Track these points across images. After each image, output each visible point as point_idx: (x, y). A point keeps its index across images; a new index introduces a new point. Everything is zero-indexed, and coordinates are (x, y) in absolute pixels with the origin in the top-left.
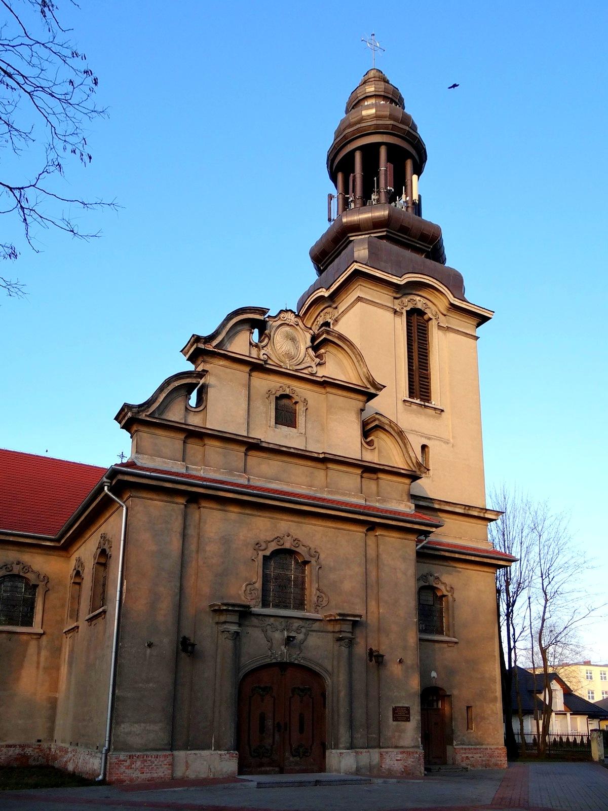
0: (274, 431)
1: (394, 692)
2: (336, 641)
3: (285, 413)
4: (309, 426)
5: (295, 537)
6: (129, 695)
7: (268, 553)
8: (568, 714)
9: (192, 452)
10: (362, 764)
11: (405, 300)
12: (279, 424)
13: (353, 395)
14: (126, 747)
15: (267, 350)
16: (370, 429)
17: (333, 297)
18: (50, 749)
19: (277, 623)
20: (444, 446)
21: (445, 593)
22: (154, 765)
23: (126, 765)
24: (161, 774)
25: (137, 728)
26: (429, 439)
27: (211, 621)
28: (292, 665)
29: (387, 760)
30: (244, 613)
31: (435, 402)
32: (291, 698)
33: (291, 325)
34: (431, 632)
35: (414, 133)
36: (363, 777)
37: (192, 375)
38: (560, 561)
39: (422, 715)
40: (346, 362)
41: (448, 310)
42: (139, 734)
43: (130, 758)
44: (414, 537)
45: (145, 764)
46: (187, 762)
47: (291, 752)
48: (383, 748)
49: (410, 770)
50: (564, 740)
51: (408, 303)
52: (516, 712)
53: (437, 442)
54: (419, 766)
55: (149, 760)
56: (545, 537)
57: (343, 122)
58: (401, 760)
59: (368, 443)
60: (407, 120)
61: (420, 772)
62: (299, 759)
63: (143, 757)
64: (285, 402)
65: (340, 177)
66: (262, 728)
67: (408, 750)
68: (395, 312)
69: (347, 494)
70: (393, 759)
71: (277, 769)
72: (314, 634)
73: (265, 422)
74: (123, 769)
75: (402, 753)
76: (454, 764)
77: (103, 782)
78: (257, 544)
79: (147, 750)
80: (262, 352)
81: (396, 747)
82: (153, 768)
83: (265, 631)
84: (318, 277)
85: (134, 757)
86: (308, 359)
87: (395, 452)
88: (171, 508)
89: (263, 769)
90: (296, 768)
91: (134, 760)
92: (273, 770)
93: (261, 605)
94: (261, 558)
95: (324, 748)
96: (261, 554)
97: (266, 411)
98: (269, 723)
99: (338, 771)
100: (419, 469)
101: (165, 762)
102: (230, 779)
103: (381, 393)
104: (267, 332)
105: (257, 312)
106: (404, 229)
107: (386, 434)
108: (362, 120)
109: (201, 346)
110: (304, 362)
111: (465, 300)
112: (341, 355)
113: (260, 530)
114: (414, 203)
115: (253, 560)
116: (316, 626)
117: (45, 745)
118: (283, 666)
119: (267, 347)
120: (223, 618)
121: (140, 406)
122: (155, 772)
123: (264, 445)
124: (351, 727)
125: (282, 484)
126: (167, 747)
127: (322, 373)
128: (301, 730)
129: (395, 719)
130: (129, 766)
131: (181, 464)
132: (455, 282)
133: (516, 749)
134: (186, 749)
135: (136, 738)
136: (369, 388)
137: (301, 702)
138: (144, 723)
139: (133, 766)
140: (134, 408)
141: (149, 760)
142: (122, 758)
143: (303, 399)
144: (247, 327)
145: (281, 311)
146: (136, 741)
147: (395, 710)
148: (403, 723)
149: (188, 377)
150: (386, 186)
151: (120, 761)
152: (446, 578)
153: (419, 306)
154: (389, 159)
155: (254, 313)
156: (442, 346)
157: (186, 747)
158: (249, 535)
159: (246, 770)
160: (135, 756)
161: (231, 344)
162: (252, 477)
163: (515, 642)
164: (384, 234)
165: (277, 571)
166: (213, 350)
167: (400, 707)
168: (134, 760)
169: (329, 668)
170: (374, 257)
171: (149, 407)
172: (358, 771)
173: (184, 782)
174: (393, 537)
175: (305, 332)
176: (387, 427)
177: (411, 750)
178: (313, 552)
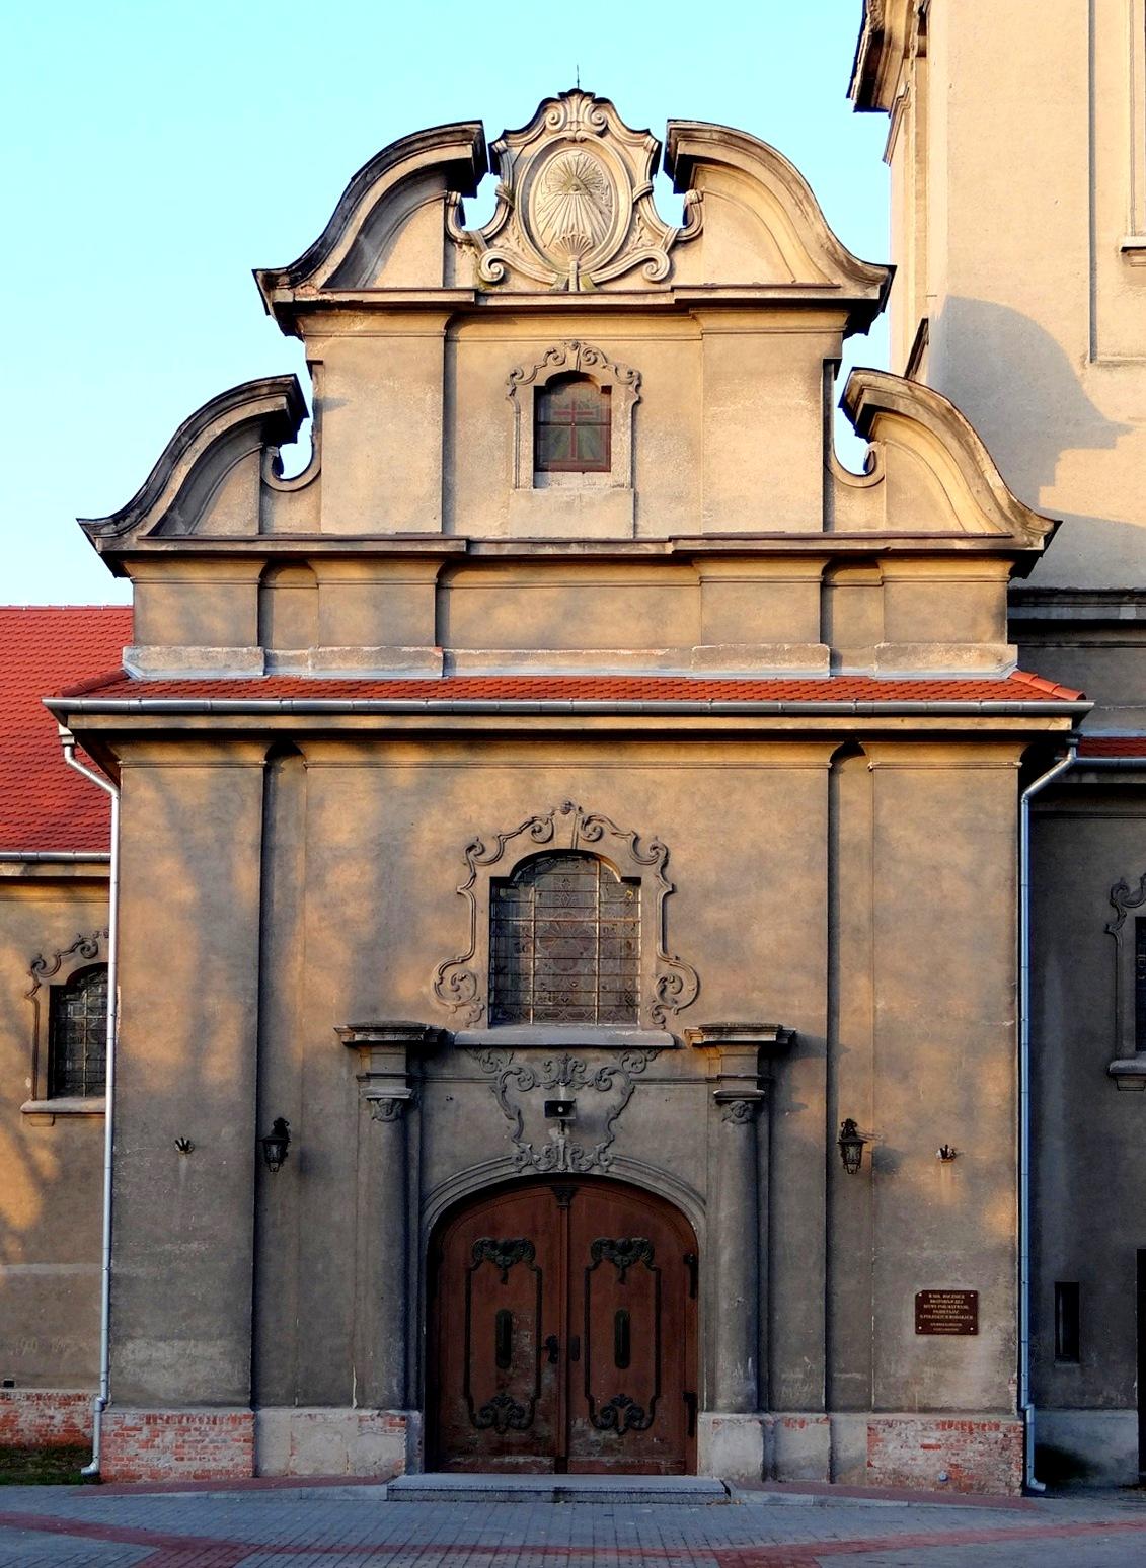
0: (530, 497)
1: (922, 1249)
2: (715, 1107)
4: (646, 455)
5: (588, 812)
6: (141, 1272)
7: (503, 869)
9: (290, 609)
10: (803, 1454)
12: (553, 470)
19: (538, 1067)
22: (207, 1440)
23: (140, 1439)
24: (226, 1464)
25: (165, 1352)
27: (345, 1074)
28: (584, 1178)
29: (890, 1448)
30: (427, 1050)
32: (588, 1270)
33: (583, 140)
37: (256, 392)
42: (171, 1367)
43: (148, 1423)
45: (186, 1437)
47: (593, 1419)
48: (877, 1410)
49: (971, 1477)
54: (1004, 1466)
55: (195, 1429)
58: (939, 1447)
61: (1007, 1484)
62: (615, 1436)
63: (180, 1422)
66: (505, 1354)
67: (966, 1418)
69: (765, 651)
70: (911, 1443)
71: (547, 1461)
72: (652, 1087)
73: (502, 475)
74: (132, 1448)
75: (943, 1426)
78: (471, 848)
79: (192, 1404)
82: (206, 1447)
85: (159, 1421)
88: (228, 779)
89: (507, 1459)
90: (605, 1459)
91: (158, 1427)
92: (534, 1463)
93: (485, 1018)
94: (483, 889)
96: (485, 874)
98: (525, 1341)
100: (1025, 525)
101: (236, 1435)
105: (448, 138)
107: (909, 428)
110: (627, 250)
112: (749, 196)
113: (482, 807)
115: (459, 893)
116: (659, 1066)
118: (565, 1185)
119: (504, 234)
120: (368, 1064)
121: (118, 517)
122: (211, 1457)
123: (484, 550)
125: (555, 656)
126: (238, 1399)
128: (623, 1358)
129: (925, 1327)
130: (148, 1442)
131: (250, 653)
134: (291, 1404)
135: (164, 1374)
136: (838, 287)
137: (622, 1281)
138: (181, 1338)
139: (158, 1441)
140: (104, 526)
141: (195, 1429)
142: (129, 1422)
143: (623, 374)
144: (434, 189)
145: (545, 104)
146: (161, 1382)
147: (922, 1300)
148: (953, 1339)
149: (247, 402)
151: (127, 1429)
155: (440, 145)
158: (449, 825)
159: (459, 1459)
160: (161, 1419)
161: (386, 260)
162: (462, 651)
166: (320, 297)
167: (942, 1293)
168: (158, 1427)
169: (700, 1185)
171: (145, 513)
174: (931, 767)
175: (629, 148)
177: (976, 1419)
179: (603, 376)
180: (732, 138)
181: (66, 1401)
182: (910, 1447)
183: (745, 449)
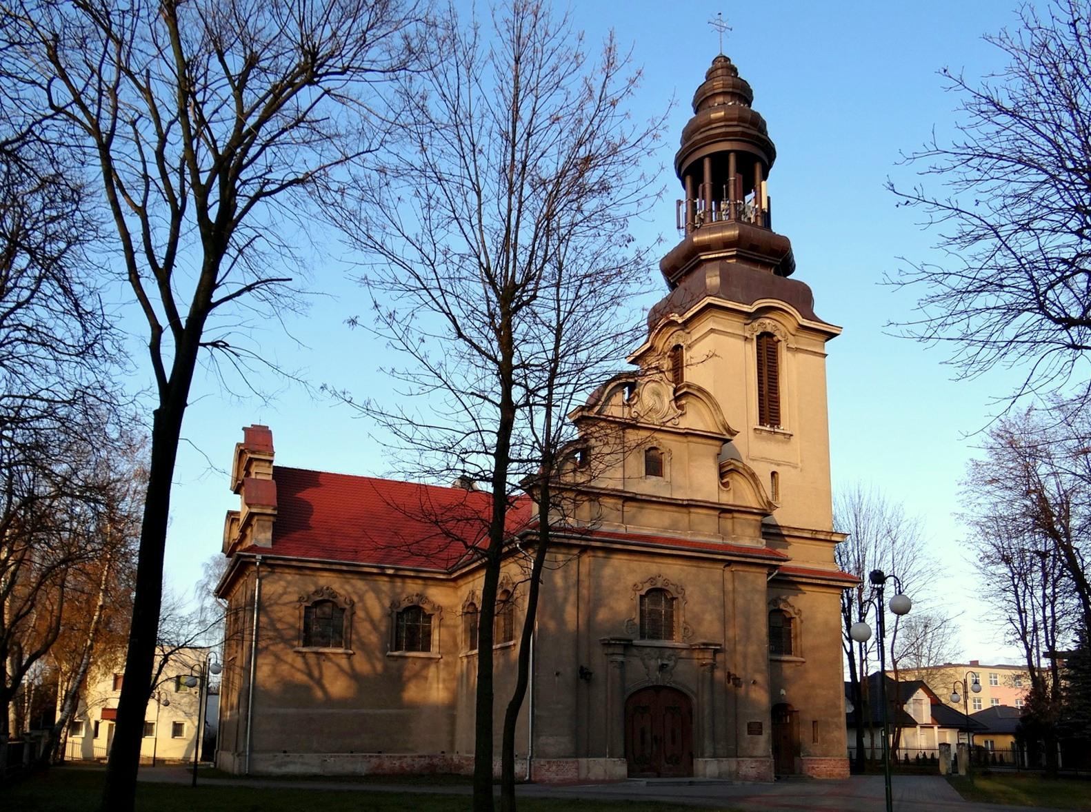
3: (654, 466)
7: (643, 593)
8: (936, 728)
11: (756, 324)
13: (710, 442)
14: (545, 756)
15: (637, 408)
16: (725, 472)
17: (686, 324)
18: (452, 759)
20: (793, 471)
21: (794, 616)
24: (570, 776)
25: (551, 740)
26: (779, 465)
28: (665, 687)
30: (627, 645)
31: (784, 426)
34: (781, 653)
35: (764, 137)
36: (722, 780)
38: (915, 568)
39: (773, 729)
40: (704, 411)
41: (797, 330)
44: (766, 571)
46: (588, 767)
50: (929, 757)
51: (757, 327)
52: (867, 725)
53: (786, 468)
56: (899, 542)
57: (691, 121)
59: (723, 484)
60: (757, 123)
64: (652, 452)
65: (688, 180)
66: (643, 742)
68: (746, 339)
74: (544, 772)
75: (756, 761)
76: (801, 773)
77: (529, 782)
80: (633, 410)
81: (750, 757)
83: (643, 660)
84: (668, 292)
86: (671, 411)
87: (745, 487)
95: (692, 756)
96: (638, 593)
97: (636, 464)
98: (648, 737)
99: (704, 776)
102: (621, 780)
103: (735, 438)
104: (636, 390)
106: (753, 247)
108: (712, 122)
109: (585, 414)
111: (814, 318)
112: (699, 405)
114: (763, 212)
117: (448, 756)
118: (658, 689)
120: (611, 650)
124: (714, 739)
127: (684, 424)
128: (674, 742)
129: (750, 733)
132: (802, 298)
133: (859, 764)
144: (619, 389)
147: (749, 725)
150: (735, 200)
152: (791, 599)
153: (769, 329)
154: (738, 170)
156: (790, 366)
157: (587, 756)
163: (867, 654)
164: (734, 253)
165: (651, 607)
169: (695, 689)
170: (725, 289)
172: (720, 775)
173: (587, 781)
176: (740, 470)
178: (679, 590)
179: (662, 450)
180: (700, 389)
181: (400, 758)
182: (749, 768)
183: (696, 477)
